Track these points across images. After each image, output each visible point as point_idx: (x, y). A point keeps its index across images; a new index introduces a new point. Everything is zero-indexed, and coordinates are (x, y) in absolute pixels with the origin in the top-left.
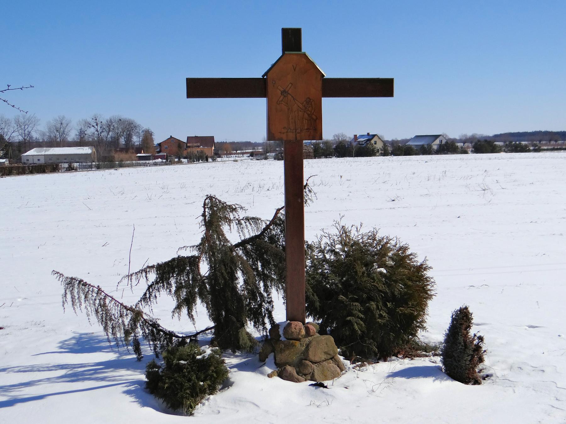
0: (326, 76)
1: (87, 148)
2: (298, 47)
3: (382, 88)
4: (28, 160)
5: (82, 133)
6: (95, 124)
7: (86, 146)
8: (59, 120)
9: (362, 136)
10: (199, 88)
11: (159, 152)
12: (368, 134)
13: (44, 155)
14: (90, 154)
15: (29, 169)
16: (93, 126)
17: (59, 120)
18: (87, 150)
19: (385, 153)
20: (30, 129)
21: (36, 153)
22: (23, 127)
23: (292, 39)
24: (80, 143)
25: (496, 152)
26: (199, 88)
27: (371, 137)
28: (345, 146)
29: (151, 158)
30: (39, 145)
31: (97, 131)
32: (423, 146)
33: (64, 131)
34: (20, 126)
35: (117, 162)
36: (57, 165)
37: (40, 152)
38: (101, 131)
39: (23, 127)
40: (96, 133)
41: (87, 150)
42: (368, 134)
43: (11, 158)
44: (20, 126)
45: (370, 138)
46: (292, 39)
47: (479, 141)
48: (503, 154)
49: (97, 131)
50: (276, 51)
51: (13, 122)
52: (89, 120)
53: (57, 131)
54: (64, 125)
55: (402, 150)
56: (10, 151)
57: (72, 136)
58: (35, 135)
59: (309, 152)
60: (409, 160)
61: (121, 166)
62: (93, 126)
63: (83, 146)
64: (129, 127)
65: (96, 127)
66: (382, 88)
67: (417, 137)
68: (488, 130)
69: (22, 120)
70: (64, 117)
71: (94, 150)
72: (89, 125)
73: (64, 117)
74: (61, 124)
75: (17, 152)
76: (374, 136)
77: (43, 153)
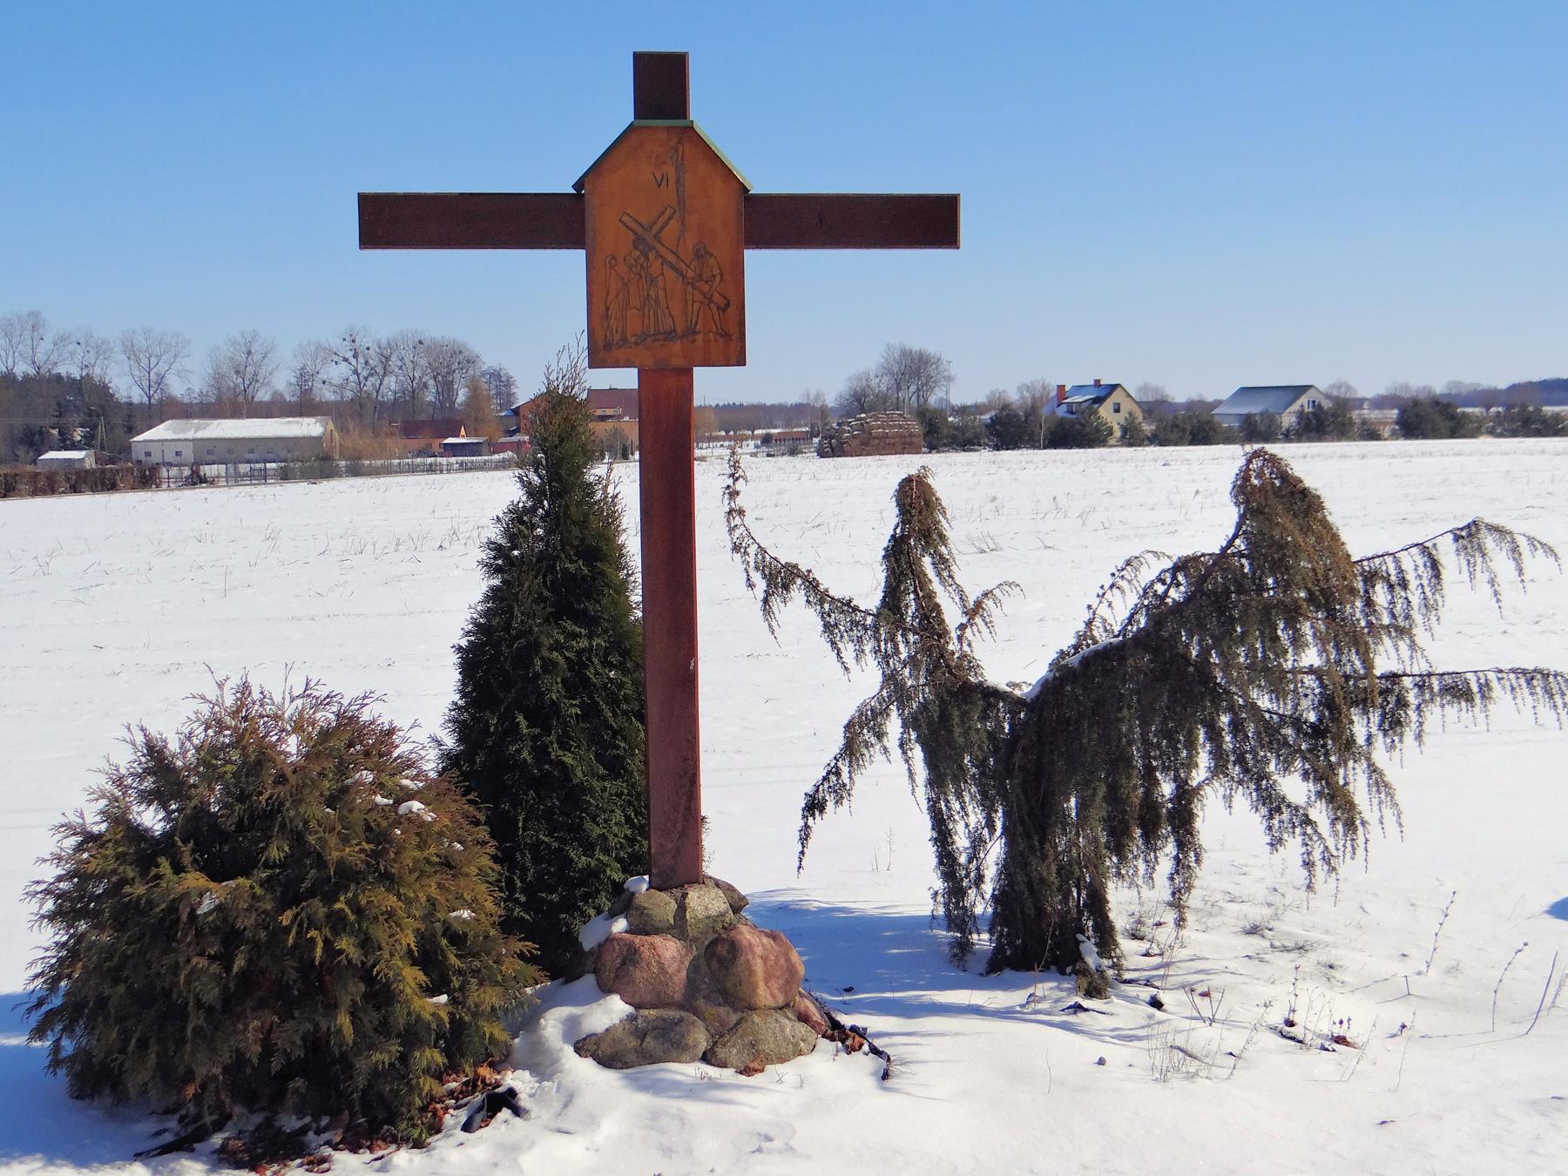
0: (759, 185)
1: (311, 420)
2: (679, 107)
3: (927, 222)
4: (148, 454)
5: (304, 377)
6: (349, 355)
7: (308, 415)
8: (242, 341)
9: (1079, 389)
10: (391, 221)
11: (512, 433)
12: (1097, 383)
13: (194, 440)
14: (318, 439)
15: (68, 480)
16: (345, 360)
17: (242, 341)
18: (310, 427)
19: (1131, 437)
20: (162, 367)
21: (170, 435)
22: (144, 363)
23: (661, 83)
24: (304, 406)
25: (1465, 437)
26: (391, 221)
27: (1104, 392)
28: (1016, 416)
29: (485, 448)
30: (185, 411)
31: (355, 372)
32: (1249, 417)
33: (255, 374)
34: (138, 361)
35: (343, 463)
36: (155, 469)
37: (183, 431)
38: (365, 373)
39: (144, 363)
40: (353, 378)
41: (310, 427)
42: (1097, 383)
43: (103, 448)
44: (138, 361)
45: (1102, 394)
46: (661, 83)
47: (1416, 403)
48: (1485, 443)
49: (355, 372)
50: (619, 111)
51: (118, 348)
52: (335, 343)
53: (237, 373)
54: (257, 357)
55: (1184, 430)
56: (101, 430)
57: (281, 382)
58: (177, 388)
59: (911, 435)
60: (1344, 456)
61: (355, 472)
62: (345, 360)
63: (301, 415)
64: (448, 362)
65: (353, 361)
66: (927, 222)
67: (1245, 391)
68: (1432, 376)
69: (141, 341)
70: (255, 334)
71: (331, 426)
72: (332, 355)
73: (255, 334)
74: (249, 353)
75: (120, 431)
76: (1114, 387)
77: (190, 435)
